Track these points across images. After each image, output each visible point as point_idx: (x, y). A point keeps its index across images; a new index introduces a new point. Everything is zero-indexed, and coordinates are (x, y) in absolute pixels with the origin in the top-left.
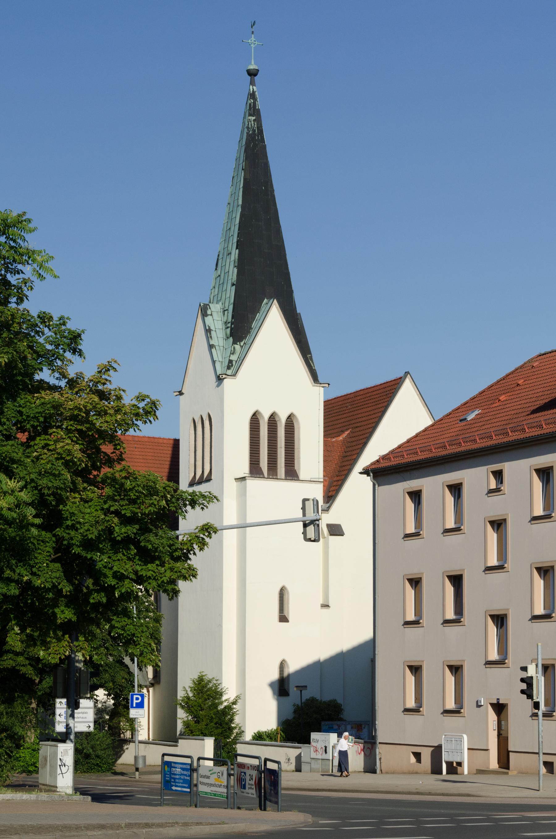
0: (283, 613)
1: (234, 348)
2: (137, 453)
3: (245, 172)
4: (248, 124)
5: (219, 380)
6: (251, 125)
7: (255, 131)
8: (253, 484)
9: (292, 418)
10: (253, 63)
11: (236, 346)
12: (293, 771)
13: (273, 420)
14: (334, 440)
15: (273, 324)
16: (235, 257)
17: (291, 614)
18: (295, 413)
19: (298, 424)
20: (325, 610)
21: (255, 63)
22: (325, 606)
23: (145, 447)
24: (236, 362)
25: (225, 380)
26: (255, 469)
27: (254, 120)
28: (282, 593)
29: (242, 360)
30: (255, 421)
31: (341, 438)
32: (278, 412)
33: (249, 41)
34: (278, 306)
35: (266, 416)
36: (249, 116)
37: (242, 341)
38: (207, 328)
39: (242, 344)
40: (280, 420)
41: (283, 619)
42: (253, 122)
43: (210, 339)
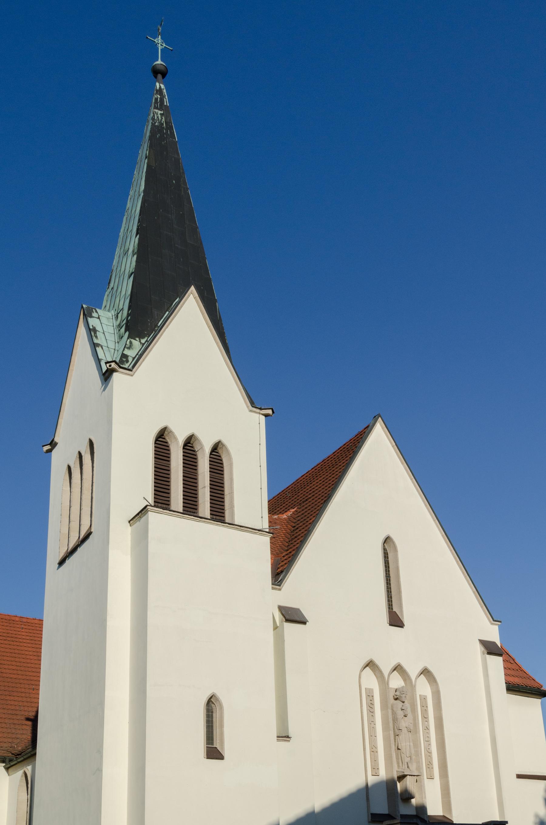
0: (212, 744)
1: (131, 342)
2: (23, 634)
3: (158, 323)
4: (154, 116)
5: (107, 376)
6: (158, 117)
7: (163, 124)
8: (156, 518)
9: (220, 451)
10: (160, 60)
11: (133, 341)
12: (30, 784)
13: (189, 445)
14: (276, 517)
15: (189, 315)
16: (134, 246)
17: (228, 744)
18: (225, 441)
19: (230, 458)
20: (283, 744)
21: (162, 60)
22: (284, 737)
23: (33, 628)
24: (134, 358)
25: (115, 374)
26: (162, 499)
27: (161, 114)
28: (211, 705)
29: (139, 357)
30: (162, 441)
31: (285, 516)
32: (198, 435)
33: (155, 41)
34: (197, 295)
35: (181, 440)
36: (154, 108)
37: (143, 338)
38: (91, 327)
39: (143, 341)
40: (202, 448)
41: (214, 753)
42: (159, 116)
43: (94, 338)
